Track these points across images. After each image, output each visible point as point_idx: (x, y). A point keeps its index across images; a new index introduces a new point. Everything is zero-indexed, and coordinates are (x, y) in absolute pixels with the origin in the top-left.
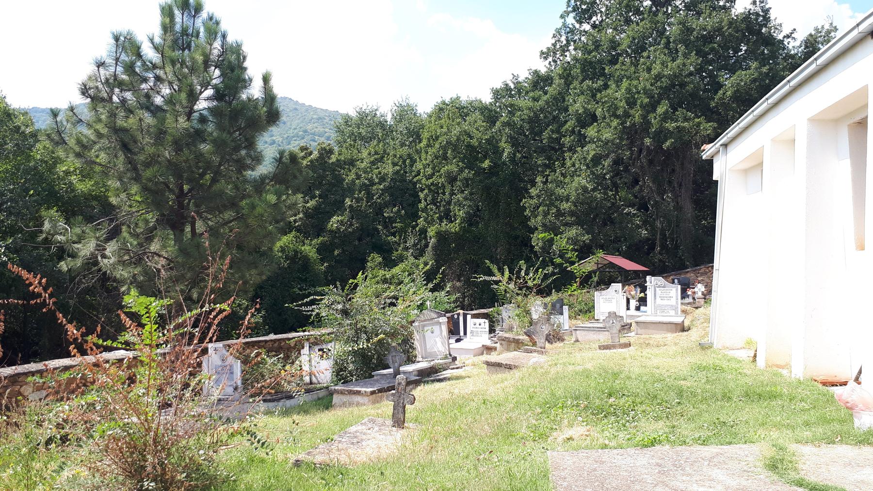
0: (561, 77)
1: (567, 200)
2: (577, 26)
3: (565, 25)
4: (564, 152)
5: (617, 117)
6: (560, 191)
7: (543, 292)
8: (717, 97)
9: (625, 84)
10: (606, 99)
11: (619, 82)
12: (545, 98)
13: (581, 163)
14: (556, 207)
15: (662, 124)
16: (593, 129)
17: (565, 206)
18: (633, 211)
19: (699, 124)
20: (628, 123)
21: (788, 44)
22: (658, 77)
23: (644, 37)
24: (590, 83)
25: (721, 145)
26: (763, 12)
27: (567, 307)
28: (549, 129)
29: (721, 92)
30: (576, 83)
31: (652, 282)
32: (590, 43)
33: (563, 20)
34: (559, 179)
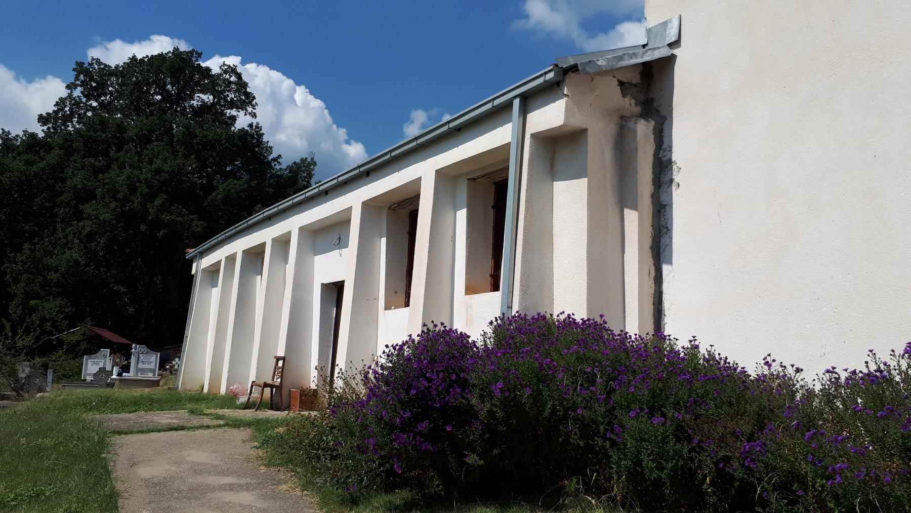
0: (61, 147)
1: (56, 271)
2: (84, 100)
3: (70, 95)
4: (56, 222)
5: (116, 199)
6: (48, 261)
7: (31, 353)
8: (210, 198)
9: (127, 171)
10: (108, 181)
11: (121, 167)
12: (41, 165)
13: (74, 237)
14: (43, 276)
15: (158, 215)
16: (91, 207)
17: (53, 276)
18: (123, 289)
19: (192, 220)
20: (127, 207)
21: (275, 166)
22: (158, 171)
23: (151, 131)
24: (93, 161)
25: (199, 252)
26: (257, 135)
27: (52, 370)
28: (42, 196)
29: (214, 194)
30: (76, 156)
31: (137, 349)
32: (96, 120)
33: (69, 91)
34: (48, 249)
